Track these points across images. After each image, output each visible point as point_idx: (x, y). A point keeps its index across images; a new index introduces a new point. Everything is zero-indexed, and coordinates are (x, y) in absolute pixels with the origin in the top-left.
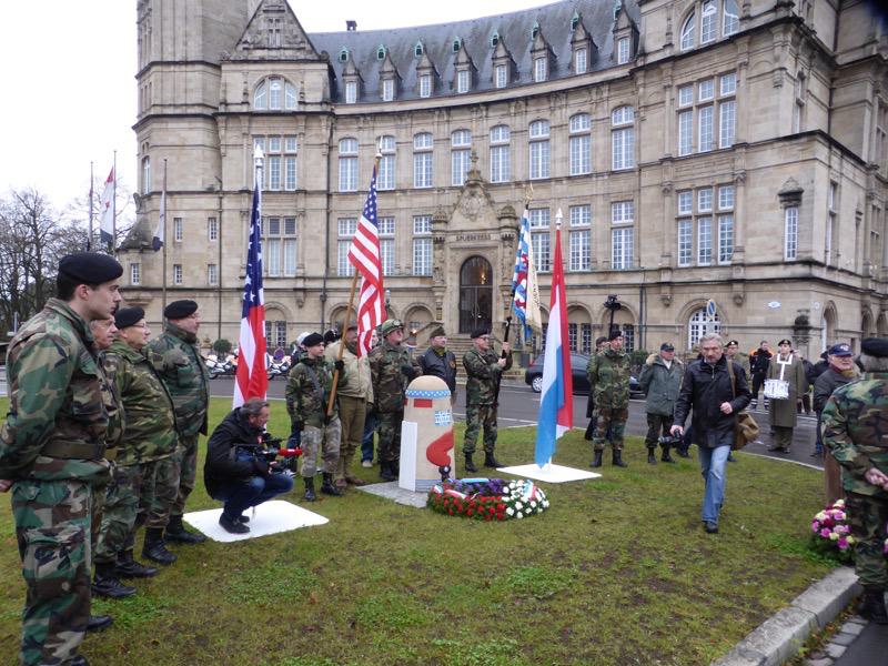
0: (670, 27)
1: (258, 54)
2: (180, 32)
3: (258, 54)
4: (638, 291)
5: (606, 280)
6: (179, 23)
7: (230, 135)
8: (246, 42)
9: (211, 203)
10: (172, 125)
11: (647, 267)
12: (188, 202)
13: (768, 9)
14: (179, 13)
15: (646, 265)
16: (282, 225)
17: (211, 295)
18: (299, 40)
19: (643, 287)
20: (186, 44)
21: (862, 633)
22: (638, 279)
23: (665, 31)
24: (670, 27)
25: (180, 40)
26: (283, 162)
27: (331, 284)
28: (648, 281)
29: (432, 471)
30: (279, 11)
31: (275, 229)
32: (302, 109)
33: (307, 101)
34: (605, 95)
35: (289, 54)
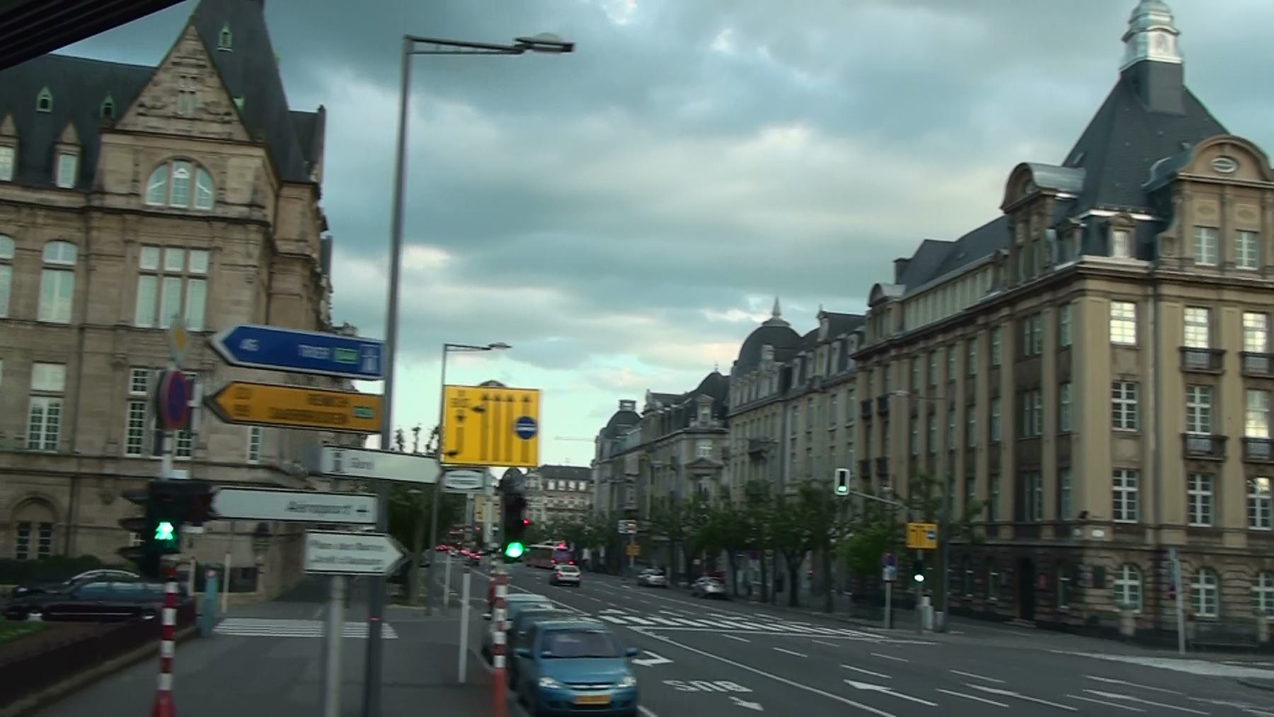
0: (137, 173)
4: (67, 481)
8: (142, 105)
11: (84, 452)
13: (244, 202)
15: (80, 449)
19: (75, 478)
21: (544, 676)
22: (71, 467)
23: (131, 178)
24: (137, 173)
28: (84, 470)
29: (561, 518)
32: (220, 212)
34: (40, 220)
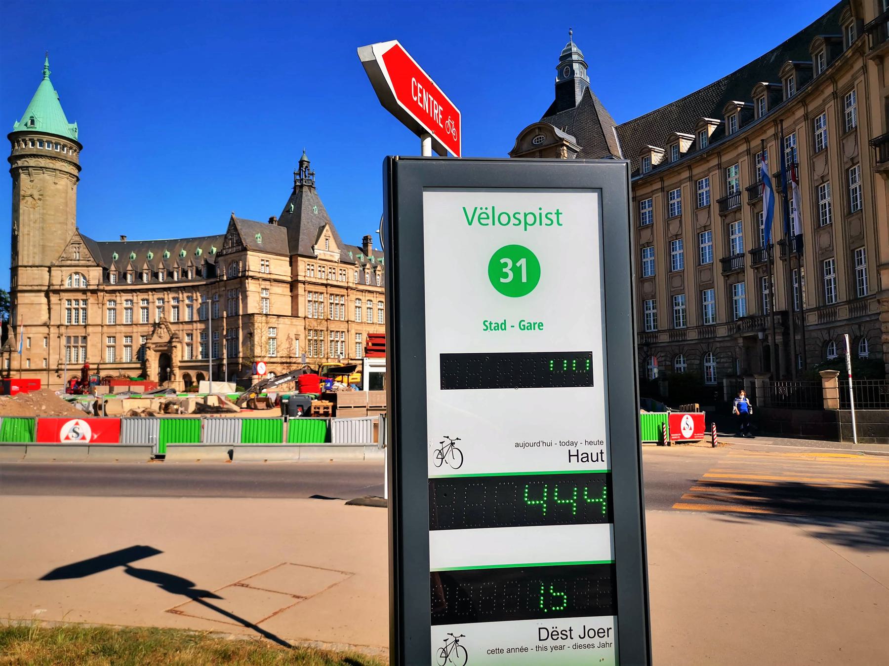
1: (69, 262)
2: (31, 252)
3: (69, 262)
5: (277, 440)
6: (31, 248)
7: (54, 298)
9: (45, 330)
10: (26, 294)
12: (34, 329)
14: (31, 243)
16: (72, 339)
17: (45, 372)
18: (88, 256)
20: (34, 257)
25: (31, 256)
26: (297, 421)
27: (101, 366)
30: (79, 244)
31: (76, 341)
33: (91, 284)
35: (82, 263)
